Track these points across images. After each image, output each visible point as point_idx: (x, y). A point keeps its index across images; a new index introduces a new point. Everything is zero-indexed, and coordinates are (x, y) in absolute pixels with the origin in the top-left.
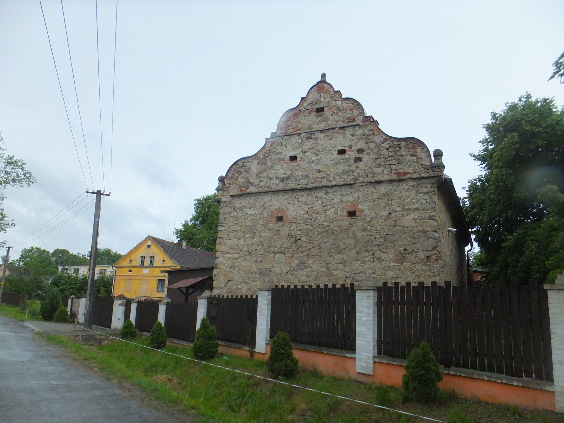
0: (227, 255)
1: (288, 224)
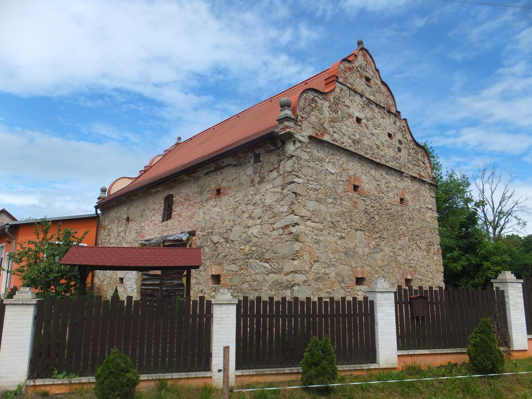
0: (309, 223)
1: (364, 197)
